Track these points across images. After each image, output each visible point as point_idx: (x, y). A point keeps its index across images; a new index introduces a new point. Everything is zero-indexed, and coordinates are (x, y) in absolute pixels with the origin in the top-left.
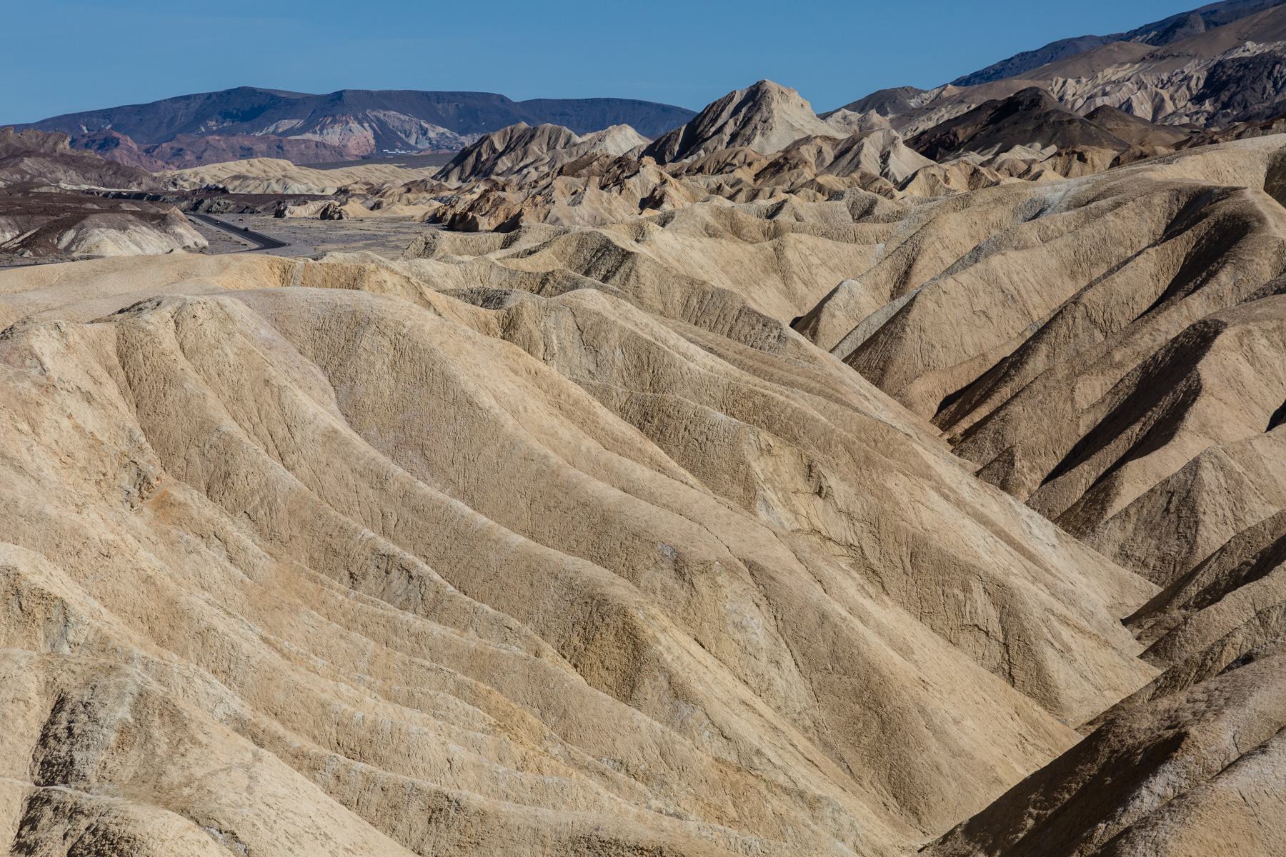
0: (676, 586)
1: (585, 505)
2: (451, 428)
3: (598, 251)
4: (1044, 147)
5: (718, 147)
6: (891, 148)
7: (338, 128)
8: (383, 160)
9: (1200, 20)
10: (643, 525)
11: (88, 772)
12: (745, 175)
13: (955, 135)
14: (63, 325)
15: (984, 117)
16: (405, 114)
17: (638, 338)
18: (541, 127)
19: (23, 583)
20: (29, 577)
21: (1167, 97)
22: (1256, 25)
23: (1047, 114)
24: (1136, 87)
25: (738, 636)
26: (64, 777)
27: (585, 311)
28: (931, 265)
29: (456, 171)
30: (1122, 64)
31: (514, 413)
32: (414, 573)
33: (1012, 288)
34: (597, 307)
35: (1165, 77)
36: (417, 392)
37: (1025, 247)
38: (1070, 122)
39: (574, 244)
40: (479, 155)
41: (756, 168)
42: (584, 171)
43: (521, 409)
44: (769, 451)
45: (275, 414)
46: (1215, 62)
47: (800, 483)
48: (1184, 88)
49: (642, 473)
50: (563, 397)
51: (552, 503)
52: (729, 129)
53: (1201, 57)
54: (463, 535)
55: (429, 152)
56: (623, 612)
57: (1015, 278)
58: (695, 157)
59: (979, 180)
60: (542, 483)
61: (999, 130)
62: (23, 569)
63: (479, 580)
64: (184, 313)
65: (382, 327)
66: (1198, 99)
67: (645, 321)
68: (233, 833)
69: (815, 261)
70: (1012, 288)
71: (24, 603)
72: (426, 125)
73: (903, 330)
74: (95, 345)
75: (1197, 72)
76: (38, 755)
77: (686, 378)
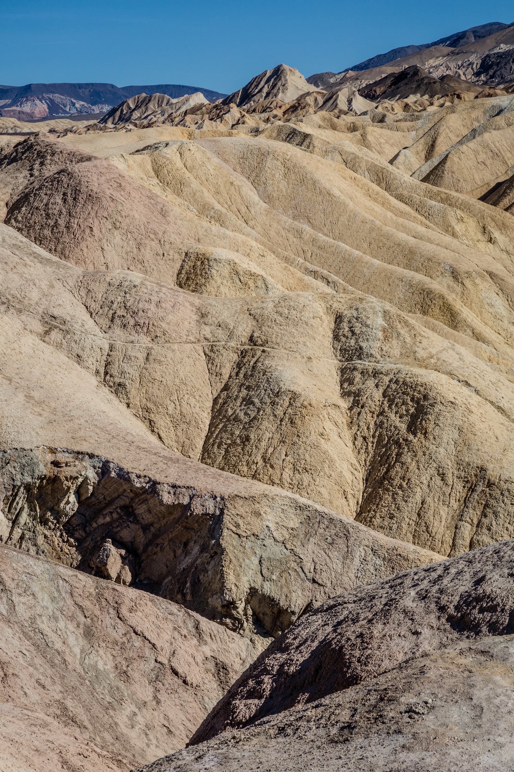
0: (455, 285)
1: (399, 245)
2: (321, 207)
3: (289, 134)
4: (421, 96)
5: (260, 99)
6: (352, 97)
7: (29, 104)
8: (54, 118)
9: (472, 35)
10: (432, 254)
11: (374, 353)
12: (279, 112)
13: (375, 91)
14: (124, 155)
15: (389, 82)
16: (63, 95)
17: (376, 166)
18: (154, 95)
19: (239, 268)
20: (241, 265)
21: (461, 74)
22: (505, 35)
23: (423, 79)
24: (445, 69)
25: (491, 310)
26: (358, 356)
27: (346, 152)
28: (445, 141)
29: (111, 119)
30: (437, 58)
31: (351, 198)
32: (330, 280)
33: (496, 150)
34: (352, 150)
35: (460, 63)
36: (300, 189)
37: (499, 129)
38: (435, 83)
39: (276, 131)
40: (122, 111)
41: (284, 109)
42: (198, 112)
43: (354, 197)
44: (462, 220)
45: (239, 200)
46: (485, 55)
47: (480, 236)
48: (470, 69)
49: (421, 229)
50: (370, 191)
51: (381, 245)
52: (265, 90)
53: (477, 53)
54: (346, 260)
55: (76, 114)
56: (442, 297)
57: (497, 144)
58: (249, 105)
59: (409, 109)
60: (374, 235)
61: (398, 88)
62: (237, 261)
63: (361, 283)
64: (183, 148)
65: (276, 156)
66: (477, 74)
67: (376, 157)
68: (466, 382)
69: (382, 141)
70: (496, 150)
71: (242, 279)
72: (74, 101)
73: (443, 173)
74: (141, 165)
75: (476, 60)
76: (336, 346)
77: (404, 185)
